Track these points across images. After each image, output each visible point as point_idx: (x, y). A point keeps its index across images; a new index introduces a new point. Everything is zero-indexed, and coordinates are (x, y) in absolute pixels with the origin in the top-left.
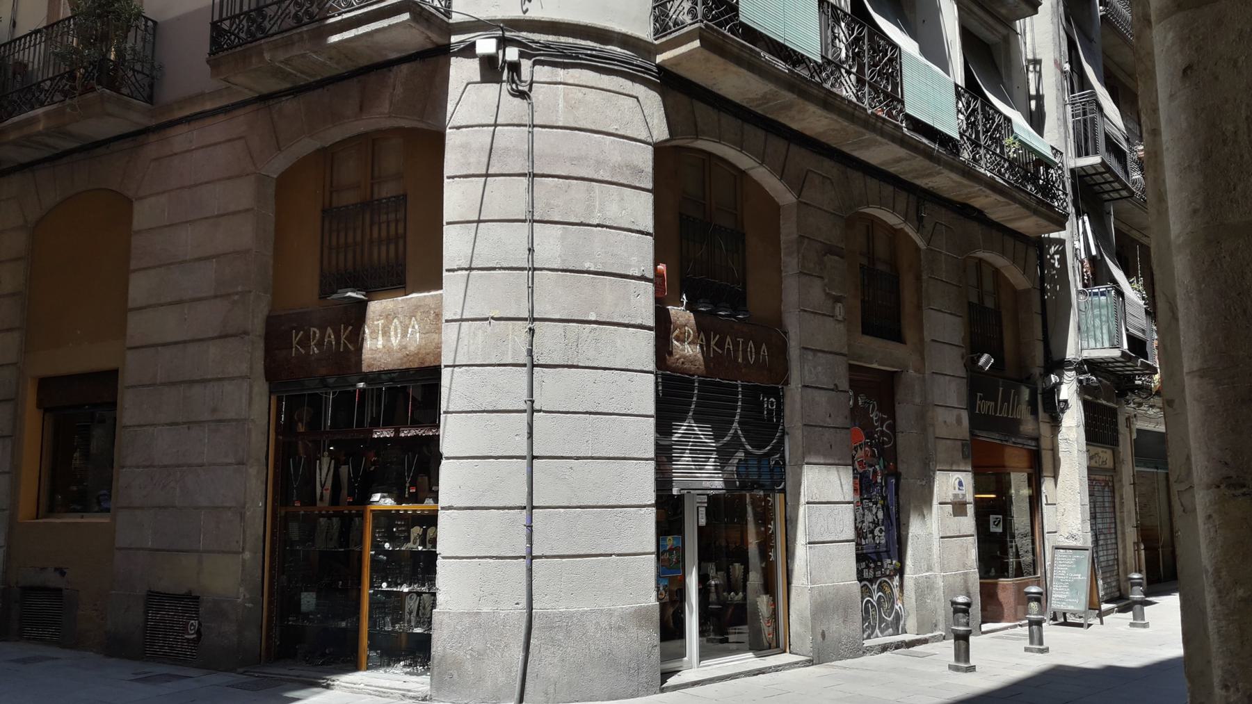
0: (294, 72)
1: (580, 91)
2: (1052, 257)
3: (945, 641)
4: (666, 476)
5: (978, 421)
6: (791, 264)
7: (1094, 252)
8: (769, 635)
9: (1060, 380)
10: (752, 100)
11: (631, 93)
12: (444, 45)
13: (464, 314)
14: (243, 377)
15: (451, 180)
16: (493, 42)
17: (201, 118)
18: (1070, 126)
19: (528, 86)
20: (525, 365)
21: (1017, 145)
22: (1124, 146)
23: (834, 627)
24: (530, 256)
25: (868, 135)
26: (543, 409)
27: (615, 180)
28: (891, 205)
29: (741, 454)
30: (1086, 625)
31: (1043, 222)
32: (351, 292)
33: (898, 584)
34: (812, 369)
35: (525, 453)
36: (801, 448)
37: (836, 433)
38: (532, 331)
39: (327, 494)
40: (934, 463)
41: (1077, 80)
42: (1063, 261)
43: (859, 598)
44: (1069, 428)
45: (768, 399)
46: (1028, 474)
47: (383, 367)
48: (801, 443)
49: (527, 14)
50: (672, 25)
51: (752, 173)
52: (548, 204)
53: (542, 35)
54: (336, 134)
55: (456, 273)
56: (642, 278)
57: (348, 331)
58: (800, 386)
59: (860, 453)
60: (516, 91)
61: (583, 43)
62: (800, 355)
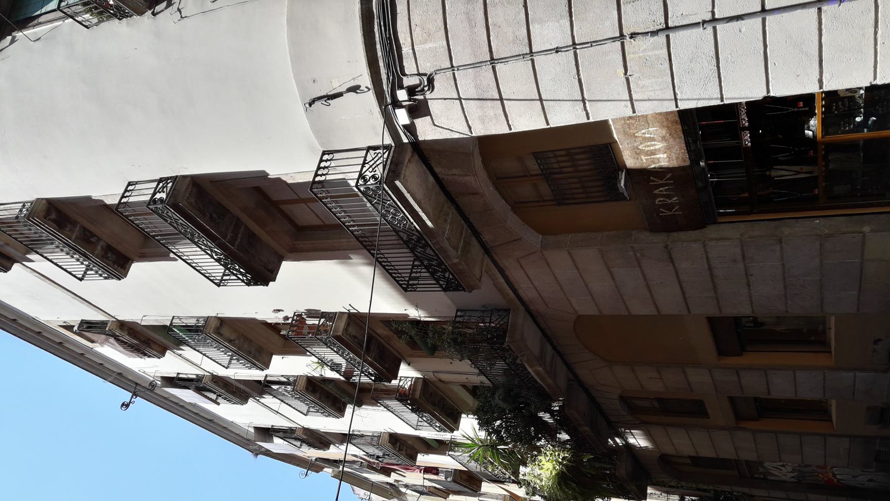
0: (462, 239)
1: (415, 30)
12: (412, 146)
13: (625, 99)
14: (704, 246)
15: (512, 127)
16: (398, 111)
17: (512, 286)
20: (668, 37)
24: (563, 50)
32: (620, 183)
38: (633, 35)
39: (806, 168)
47: (684, 150)
52: (514, 42)
54: (500, 206)
55: (589, 111)
57: (655, 179)
60: (429, 86)
61: (378, 35)
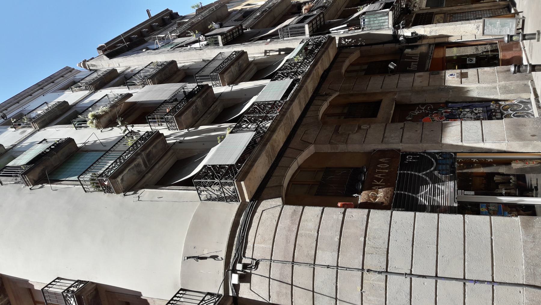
2: (346, 42)
3: (534, 80)
4: (448, 209)
5: (421, 68)
6: (341, 148)
7: (346, 25)
8: (534, 163)
9: (402, 36)
10: (269, 161)
11: (261, 213)
16: (233, 275)
18: (292, 38)
19: (254, 260)
20: (386, 276)
21: (298, 57)
22: (302, 17)
23: (529, 131)
24: (331, 267)
25: (288, 114)
26: (410, 269)
27: (298, 223)
28: (319, 106)
29: (436, 173)
30: (523, 18)
31: (331, 45)
33: (504, 102)
34: (393, 138)
35: (434, 280)
36: (433, 144)
37: (425, 128)
38: (369, 271)
40: (441, 86)
41: (274, 36)
42: (348, 38)
43: (512, 119)
44: (425, 31)
45: (407, 159)
46: (447, 48)
48: (430, 144)
49: (223, 258)
50: (234, 194)
51: (300, 164)
53: (233, 252)
56: (344, 213)
58: (401, 144)
59: (436, 118)
60: (255, 266)
61: (238, 234)
62: (386, 144)
